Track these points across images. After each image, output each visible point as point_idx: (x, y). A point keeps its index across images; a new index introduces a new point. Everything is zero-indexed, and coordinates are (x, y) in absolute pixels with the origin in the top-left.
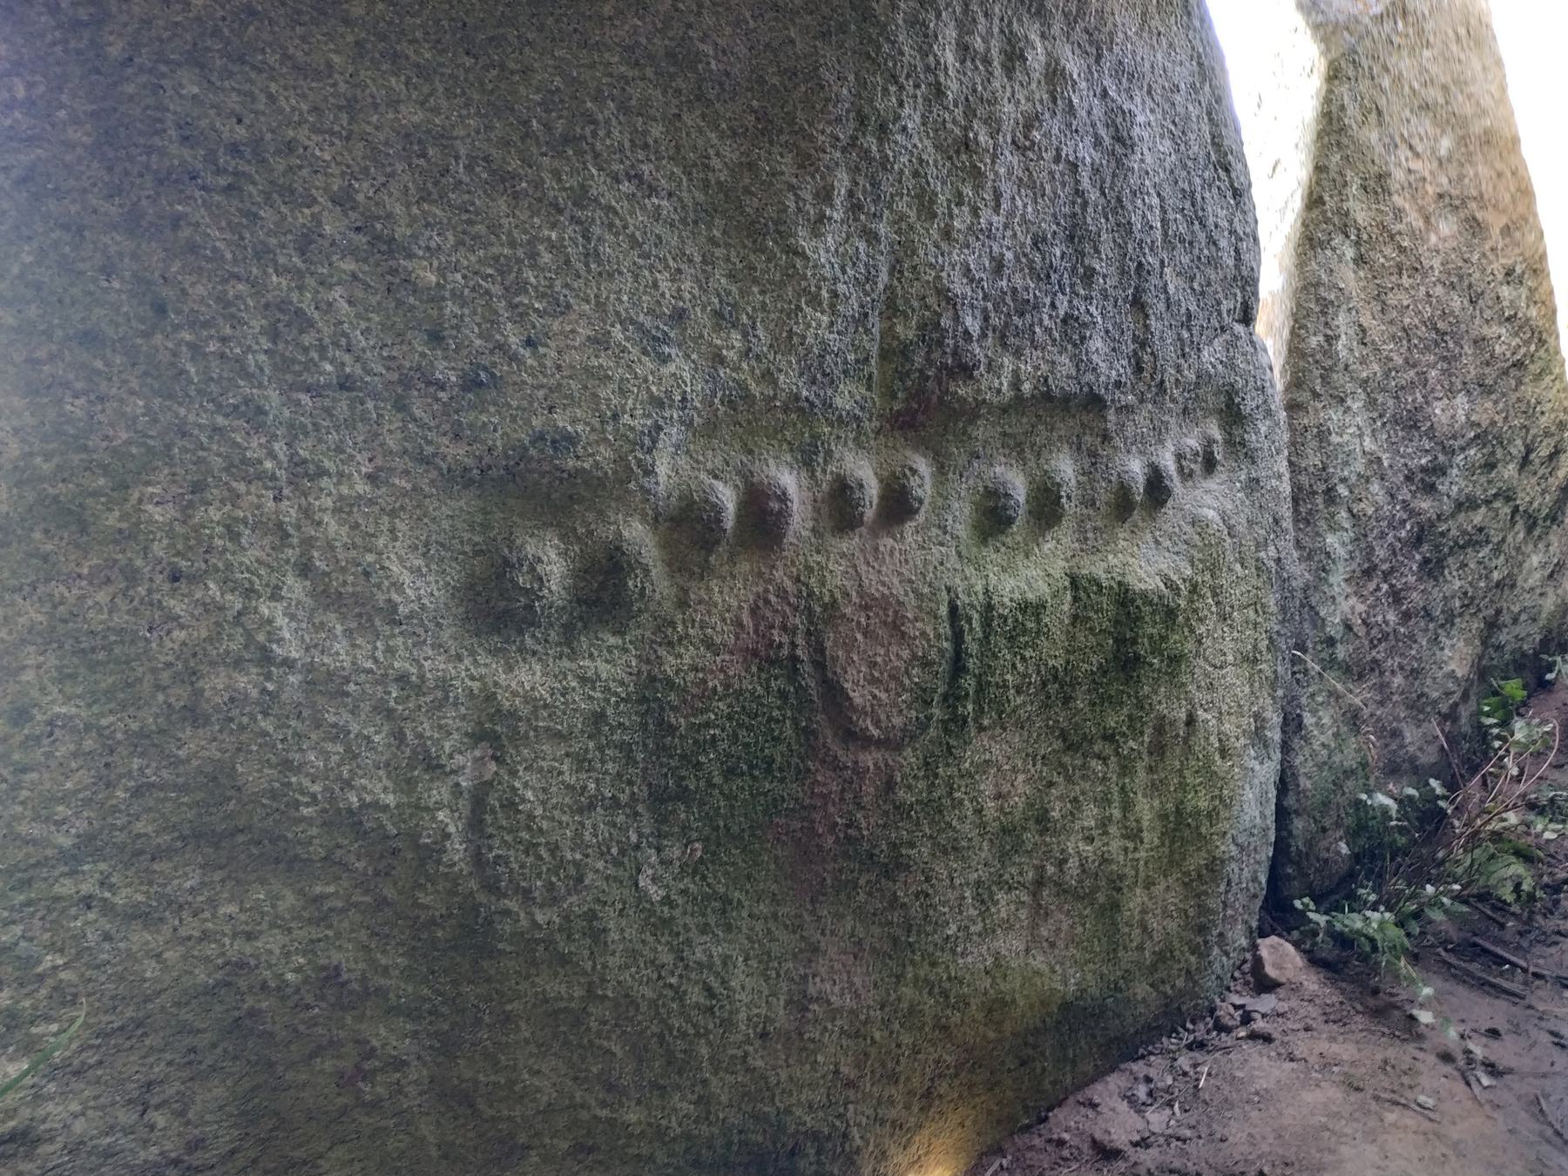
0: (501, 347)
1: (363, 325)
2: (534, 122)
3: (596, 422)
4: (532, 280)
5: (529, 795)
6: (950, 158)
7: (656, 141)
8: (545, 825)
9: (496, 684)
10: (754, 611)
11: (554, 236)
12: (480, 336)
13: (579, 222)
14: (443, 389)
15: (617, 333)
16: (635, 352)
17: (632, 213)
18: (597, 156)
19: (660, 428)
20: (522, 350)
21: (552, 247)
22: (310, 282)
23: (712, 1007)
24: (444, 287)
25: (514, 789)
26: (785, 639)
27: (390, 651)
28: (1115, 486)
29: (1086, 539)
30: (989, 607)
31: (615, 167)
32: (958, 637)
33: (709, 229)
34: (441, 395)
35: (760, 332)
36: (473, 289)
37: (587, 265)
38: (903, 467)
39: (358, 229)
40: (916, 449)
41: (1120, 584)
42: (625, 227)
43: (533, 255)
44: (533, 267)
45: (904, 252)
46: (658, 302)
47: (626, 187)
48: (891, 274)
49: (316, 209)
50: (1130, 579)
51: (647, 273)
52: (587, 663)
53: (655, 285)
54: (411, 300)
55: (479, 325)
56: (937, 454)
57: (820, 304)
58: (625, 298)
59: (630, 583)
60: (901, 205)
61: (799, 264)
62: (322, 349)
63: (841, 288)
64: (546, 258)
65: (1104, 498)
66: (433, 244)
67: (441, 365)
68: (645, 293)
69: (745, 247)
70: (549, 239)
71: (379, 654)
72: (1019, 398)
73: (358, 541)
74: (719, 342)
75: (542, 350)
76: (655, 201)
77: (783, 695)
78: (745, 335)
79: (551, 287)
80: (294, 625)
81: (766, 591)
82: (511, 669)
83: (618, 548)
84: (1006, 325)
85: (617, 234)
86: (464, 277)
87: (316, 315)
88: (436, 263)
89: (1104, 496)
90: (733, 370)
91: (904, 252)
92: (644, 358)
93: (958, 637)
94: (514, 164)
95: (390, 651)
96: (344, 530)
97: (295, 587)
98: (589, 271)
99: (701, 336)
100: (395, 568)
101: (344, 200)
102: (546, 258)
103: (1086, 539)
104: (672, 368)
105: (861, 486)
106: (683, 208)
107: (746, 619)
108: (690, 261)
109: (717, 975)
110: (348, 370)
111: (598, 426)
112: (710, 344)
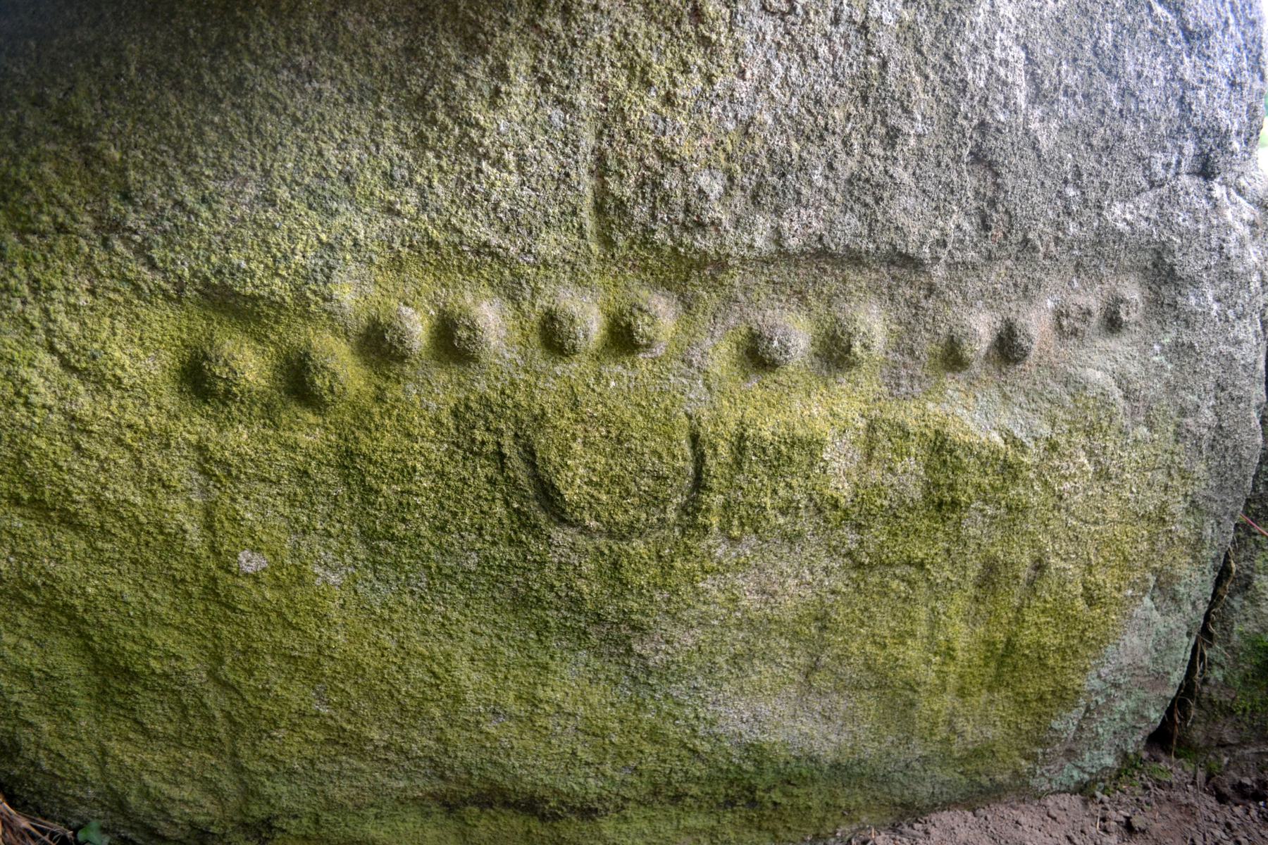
0: (180, 204)
1: (68, 188)
2: (191, 31)
3: (270, 262)
4: (201, 154)
5: (249, 515)
6: (669, 29)
7: (311, 36)
8: (264, 538)
9: (208, 439)
10: (455, 413)
11: (216, 119)
12: (162, 196)
13: (239, 107)
14: (136, 233)
15: (283, 193)
16: (301, 208)
17: (292, 97)
18: (252, 53)
19: (331, 268)
20: (197, 206)
21: (216, 127)
22: (24, 161)
23: (438, 685)
24: (126, 162)
25: (237, 511)
26: (489, 437)
27: (122, 407)
28: (944, 341)
29: (898, 385)
30: (742, 438)
31: (271, 61)
32: (699, 459)
33: (376, 105)
34: (136, 237)
35: (440, 190)
36: (152, 162)
37: (250, 140)
38: (633, 305)
39: (55, 122)
40: (654, 288)
41: (937, 432)
42: (285, 109)
43: (201, 135)
44: (202, 143)
45: (612, 117)
46: (324, 169)
47: (284, 75)
48: (599, 135)
49: (20, 110)
50: (950, 429)
51: (311, 143)
52: (287, 434)
53: (320, 154)
54: (103, 170)
55: (159, 188)
56: (682, 297)
57: (505, 166)
58: (290, 165)
59: (318, 382)
60: (606, 75)
61: (474, 133)
62: (40, 206)
63: (530, 151)
64: (212, 136)
65: (929, 347)
66: (115, 130)
67: (132, 216)
68: (310, 160)
69: (415, 120)
70: (212, 122)
71: (114, 408)
72: (784, 254)
73: (87, 334)
74: (392, 198)
75: (215, 206)
76: (316, 85)
77: (492, 481)
78: (422, 193)
79: (219, 158)
80: (47, 384)
81: (467, 399)
82: (221, 430)
83: (307, 354)
84: (759, 185)
85: (278, 115)
86: (144, 153)
87: (31, 183)
88: (118, 144)
89: (927, 346)
90: (411, 220)
91: (612, 117)
92: (310, 212)
93: (699, 459)
94: (177, 64)
95: (122, 407)
96: (76, 327)
97: (45, 359)
98: (253, 144)
99: (372, 194)
100: (117, 354)
101: (40, 102)
102: (212, 136)
103: (898, 385)
104: (339, 220)
105: (572, 321)
106: (348, 89)
107: (446, 418)
108: (357, 132)
109: (439, 664)
110: (60, 220)
111: (270, 264)
112: (381, 201)
